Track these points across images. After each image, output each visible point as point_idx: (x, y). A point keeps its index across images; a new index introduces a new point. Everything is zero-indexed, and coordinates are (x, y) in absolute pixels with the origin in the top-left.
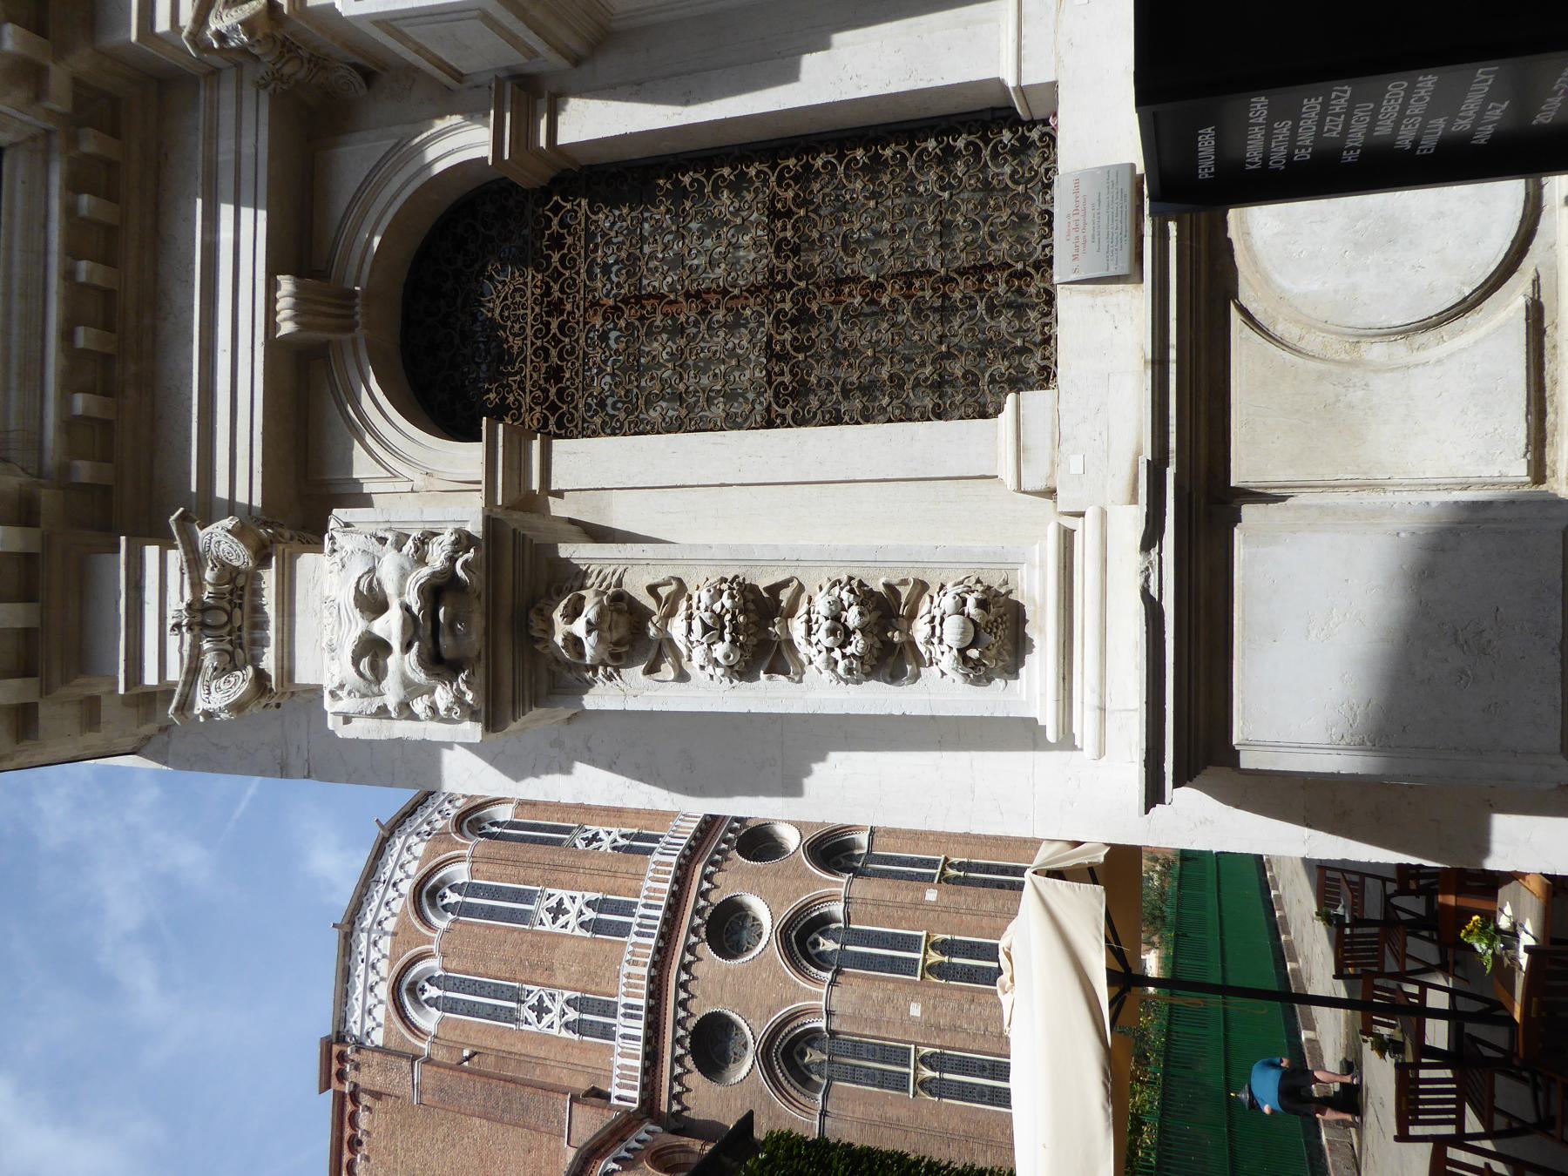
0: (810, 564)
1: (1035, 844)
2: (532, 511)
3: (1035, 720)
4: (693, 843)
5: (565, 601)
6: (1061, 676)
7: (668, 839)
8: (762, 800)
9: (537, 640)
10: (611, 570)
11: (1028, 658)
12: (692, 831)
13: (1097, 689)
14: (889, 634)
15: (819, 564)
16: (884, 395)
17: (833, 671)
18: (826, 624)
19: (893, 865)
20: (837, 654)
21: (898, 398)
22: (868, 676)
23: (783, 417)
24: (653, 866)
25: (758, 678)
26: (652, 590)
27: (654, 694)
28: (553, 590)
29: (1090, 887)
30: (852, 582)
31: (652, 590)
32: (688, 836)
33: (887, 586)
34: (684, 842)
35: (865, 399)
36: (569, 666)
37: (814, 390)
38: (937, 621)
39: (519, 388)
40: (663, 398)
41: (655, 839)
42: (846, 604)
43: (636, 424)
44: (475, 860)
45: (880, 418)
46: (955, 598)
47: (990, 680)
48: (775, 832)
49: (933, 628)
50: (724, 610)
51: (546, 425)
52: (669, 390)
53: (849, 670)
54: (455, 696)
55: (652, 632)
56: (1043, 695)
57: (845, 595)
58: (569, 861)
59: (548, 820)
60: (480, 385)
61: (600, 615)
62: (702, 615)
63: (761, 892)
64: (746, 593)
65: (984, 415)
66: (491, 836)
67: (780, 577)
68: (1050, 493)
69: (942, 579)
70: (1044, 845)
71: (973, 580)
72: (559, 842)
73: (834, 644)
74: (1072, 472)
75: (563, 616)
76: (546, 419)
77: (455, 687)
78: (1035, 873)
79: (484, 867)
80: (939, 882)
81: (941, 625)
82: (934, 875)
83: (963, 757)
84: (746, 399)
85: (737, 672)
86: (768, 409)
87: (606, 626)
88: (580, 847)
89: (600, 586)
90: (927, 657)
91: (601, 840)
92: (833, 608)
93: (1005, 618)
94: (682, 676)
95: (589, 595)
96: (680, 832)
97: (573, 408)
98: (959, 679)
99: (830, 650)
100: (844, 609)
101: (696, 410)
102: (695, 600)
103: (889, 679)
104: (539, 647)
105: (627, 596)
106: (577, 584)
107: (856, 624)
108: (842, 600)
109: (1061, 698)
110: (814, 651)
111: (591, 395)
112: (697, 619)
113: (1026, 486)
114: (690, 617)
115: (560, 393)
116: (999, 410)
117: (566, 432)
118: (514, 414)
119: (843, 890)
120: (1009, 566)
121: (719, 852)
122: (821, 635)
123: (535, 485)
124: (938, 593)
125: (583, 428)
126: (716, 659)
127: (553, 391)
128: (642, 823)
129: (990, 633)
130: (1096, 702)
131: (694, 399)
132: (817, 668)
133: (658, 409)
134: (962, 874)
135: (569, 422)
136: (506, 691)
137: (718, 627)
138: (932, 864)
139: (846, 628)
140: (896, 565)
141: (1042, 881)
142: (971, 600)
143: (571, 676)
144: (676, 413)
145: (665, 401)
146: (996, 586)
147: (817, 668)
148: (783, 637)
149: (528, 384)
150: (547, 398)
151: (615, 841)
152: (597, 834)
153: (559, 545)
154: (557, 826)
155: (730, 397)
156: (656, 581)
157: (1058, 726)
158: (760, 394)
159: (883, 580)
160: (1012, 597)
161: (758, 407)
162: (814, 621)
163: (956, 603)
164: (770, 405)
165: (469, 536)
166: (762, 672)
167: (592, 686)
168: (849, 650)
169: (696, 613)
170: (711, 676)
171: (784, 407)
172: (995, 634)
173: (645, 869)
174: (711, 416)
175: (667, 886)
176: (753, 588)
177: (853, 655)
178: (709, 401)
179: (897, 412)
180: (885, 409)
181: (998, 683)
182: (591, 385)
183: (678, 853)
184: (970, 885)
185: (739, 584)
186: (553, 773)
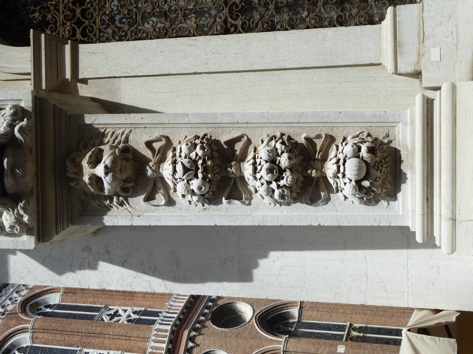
0: (255, 125)
1: (408, 311)
2: (66, 93)
3: (408, 228)
4: (182, 316)
5: (90, 153)
6: (426, 198)
7: (165, 314)
8: (226, 284)
9: (72, 180)
10: (120, 131)
11: (403, 186)
12: (181, 308)
13: (450, 207)
14: (309, 172)
15: (260, 125)
16: (304, 10)
17: (272, 197)
18: (266, 166)
19: (316, 329)
20: (274, 185)
21: (313, 12)
22: (295, 200)
23: (236, 26)
24: (155, 332)
25: (221, 203)
26: (149, 144)
27: (152, 214)
28: (81, 146)
29: (446, 340)
30: (284, 137)
31: (149, 144)
32: (178, 312)
33: (307, 139)
34: (175, 316)
35: (291, 13)
36: (94, 197)
37: (256, 8)
38: (341, 162)
39: (55, 9)
40: (154, 15)
41: (156, 314)
42: (280, 152)
43: (136, 33)
44: (35, 331)
45: (301, 26)
46: (353, 146)
47: (377, 202)
48: (236, 308)
49: (339, 167)
50: (198, 158)
51: (74, 35)
52: (158, 10)
53: (282, 196)
54: (16, 218)
55: (149, 172)
56: (413, 211)
57: (278, 146)
58: (98, 330)
59: (84, 303)
60: (28, 8)
61: (114, 162)
62: (182, 161)
63: (227, 348)
64: (212, 146)
65: (372, 22)
66: (46, 315)
67: (235, 135)
68: (417, 74)
69: (344, 133)
70: (415, 312)
71: (365, 134)
72: (92, 317)
73: (272, 178)
74: (433, 59)
75: (89, 163)
76: (74, 30)
77: (16, 212)
78: (409, 330)
79: (41, 336)
80: (346, 340)
81: (344, 164)
82: (342, 336)
83: (360, 254)
84: (210, 15)
85: (207, 198)
86: (225, 21)
87: (117, 169)
88: (106, 321)
89: (114, 143)
90: (334, 186)
91: (120, 315)
92: (271, 155)
93: (387, 160)
94: (170, 202)
95: (106, 148)
96: (172, 309)
97: (92, 23)
98: (357, 201)
99: (269, 183)
100: (278, 155)
101: (177, 23)
102: (178, 151)
103: (309, 202)
104: (72, 184)
105: (132, 149)
106: (97, 142)
107: (286, 165)
108: (277, 149)
109: (426, 213)
110: (258, 183)
111: (104, 14)
112: (180, 163)
113: (401, 70)
114: (174, 163)
115: (83, 12)
116: (382, 18)
117: (88, 40)
118: (52, 27)
119: (282, 346)
120: (390, 124)
121: (199, 322)
122: (263, 174)
123: (68, 75)
124: (342, 143)
125: (100, 37)
126: (193, 190)
127: (78, 11)
128: (148, 303)
129: (377, 170)
130: (450, 216)
131: (175, 15)
132: (261, 195)
133: (151, 22)
134: (361, 335)
135: (91, 32)
136: (51, 214)
137: (194, 168)
138: (341, 328)
139: (280, 168)
140: (312, 125)
141: (413, 335)
142: (364, 148)
143: (95, 204)
144: (162, 25)
145: (155, 17)
146: (381, 138)
147: (261, 195)
148: (238, 175)
149: (61, 7)
150: (74, 16)
151: (130, 316)
152: (110, 319)
153: (85, 115)
154: (90, 307)
155: (200, 13)
156: (151, 138)
157: (423, 231)
158: (219, 11)
159: (304, 135)
160: (392, 145)
161: (218, 20)
162: (258, 163)
163: (354, 150)
164: (226, 18)
165: (23, 109)
166: (224, 198)
167: (109, 210)
168: (282, 183)
169: (179, 159)
170: (190, 202)
171: (236, 19)
172: (381, 170)
173: (150, 334)
174: (186, 26)
175: (164, 346)
176: (217, 142)
177: (285, 186)
178: (185, 16)
179: (313, 22)
180: (304, 20)
181: (383, 203)
182: (104, 7)
183: (171, 323)
184: (367, 342)
185: (207, 140)
186: (84, 269)
